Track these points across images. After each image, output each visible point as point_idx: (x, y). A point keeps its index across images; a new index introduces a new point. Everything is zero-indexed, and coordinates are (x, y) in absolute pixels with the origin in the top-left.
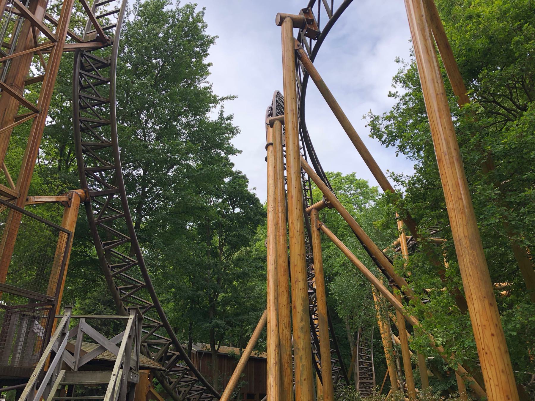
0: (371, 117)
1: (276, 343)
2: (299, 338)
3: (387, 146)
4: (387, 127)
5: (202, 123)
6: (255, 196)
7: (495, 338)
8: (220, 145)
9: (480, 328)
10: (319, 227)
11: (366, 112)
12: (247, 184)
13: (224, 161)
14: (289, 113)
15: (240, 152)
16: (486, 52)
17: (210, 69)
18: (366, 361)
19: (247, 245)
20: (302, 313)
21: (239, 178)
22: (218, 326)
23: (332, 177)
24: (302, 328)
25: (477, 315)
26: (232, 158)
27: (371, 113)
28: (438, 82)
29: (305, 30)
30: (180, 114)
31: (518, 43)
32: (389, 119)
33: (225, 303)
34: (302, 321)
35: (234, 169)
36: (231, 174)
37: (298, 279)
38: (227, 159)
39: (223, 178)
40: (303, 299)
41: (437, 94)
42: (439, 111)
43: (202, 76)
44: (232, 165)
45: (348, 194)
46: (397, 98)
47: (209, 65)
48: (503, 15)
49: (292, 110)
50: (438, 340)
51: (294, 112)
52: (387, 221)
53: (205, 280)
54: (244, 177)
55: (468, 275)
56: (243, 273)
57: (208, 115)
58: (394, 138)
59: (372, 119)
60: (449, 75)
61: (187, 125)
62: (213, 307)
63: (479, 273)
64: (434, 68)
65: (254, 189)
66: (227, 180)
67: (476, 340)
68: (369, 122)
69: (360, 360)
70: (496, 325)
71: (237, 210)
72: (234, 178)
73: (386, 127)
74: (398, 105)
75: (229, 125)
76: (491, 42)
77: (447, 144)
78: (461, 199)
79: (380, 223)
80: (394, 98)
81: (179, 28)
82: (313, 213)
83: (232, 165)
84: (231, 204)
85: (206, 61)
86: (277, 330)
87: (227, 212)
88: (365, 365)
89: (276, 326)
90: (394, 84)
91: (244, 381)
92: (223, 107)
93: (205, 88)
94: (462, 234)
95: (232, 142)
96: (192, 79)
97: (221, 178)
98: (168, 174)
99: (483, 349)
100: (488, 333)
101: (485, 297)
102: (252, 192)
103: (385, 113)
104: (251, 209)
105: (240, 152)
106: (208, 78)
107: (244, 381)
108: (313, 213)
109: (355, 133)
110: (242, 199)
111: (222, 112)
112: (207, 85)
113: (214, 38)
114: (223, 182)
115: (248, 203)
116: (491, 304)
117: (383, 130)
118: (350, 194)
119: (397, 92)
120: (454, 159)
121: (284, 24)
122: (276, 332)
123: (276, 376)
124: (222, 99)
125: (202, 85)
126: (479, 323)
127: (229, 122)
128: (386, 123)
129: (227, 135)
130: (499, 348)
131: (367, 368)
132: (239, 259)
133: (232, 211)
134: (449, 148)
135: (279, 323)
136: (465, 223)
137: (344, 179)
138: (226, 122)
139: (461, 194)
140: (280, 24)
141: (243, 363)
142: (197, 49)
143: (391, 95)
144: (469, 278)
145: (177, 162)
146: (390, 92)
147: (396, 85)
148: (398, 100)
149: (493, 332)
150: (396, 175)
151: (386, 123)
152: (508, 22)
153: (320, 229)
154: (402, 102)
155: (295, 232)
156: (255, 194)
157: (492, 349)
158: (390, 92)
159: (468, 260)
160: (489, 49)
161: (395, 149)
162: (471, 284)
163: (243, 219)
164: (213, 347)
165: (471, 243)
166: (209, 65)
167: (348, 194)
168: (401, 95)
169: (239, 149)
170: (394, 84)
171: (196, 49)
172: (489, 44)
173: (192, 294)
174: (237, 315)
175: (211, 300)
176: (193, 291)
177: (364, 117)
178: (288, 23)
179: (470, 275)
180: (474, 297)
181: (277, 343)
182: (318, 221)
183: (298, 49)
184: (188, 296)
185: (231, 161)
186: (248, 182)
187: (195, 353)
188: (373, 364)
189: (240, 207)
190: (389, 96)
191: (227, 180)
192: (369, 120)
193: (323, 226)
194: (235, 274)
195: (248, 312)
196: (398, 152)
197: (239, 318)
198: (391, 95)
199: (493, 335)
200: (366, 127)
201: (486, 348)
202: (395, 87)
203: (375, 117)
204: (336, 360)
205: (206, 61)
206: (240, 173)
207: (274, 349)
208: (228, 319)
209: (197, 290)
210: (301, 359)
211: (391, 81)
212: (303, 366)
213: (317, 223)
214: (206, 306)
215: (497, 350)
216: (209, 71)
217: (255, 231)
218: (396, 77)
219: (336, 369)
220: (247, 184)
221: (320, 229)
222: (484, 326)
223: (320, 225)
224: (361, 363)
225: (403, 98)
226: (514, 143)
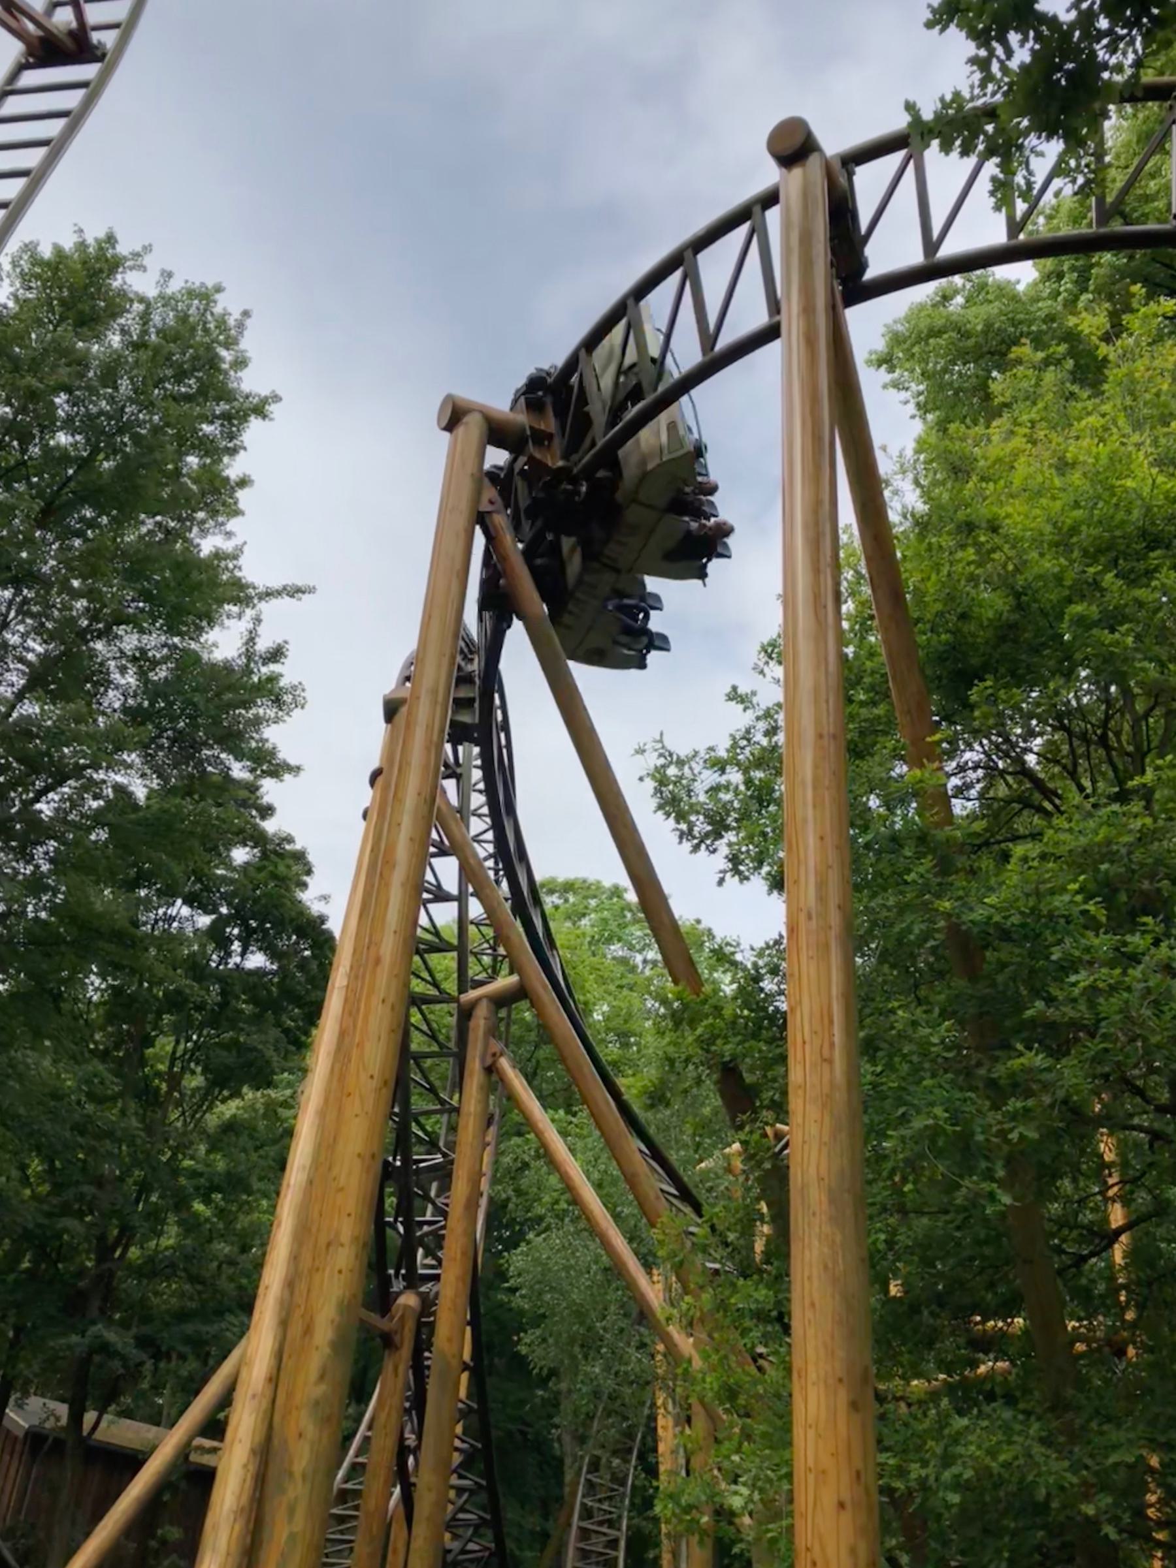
0: (661, 755)
1: (257, 1439)
2: (300, 1435)
3: (696, 848)
4: (714, 790)
5: (188, 662)
6: (323, 922)
7: (846, 1517)
8: (233, 741)
9: (811, 1478)
10: (489, 1061)
11: (647, 737)
12: (305, 878)
13: (244, 794)
14: (422, 699)
15: (296, 770)
16: (1006, 632)
17: (243, 497)
18: (604, 1529)
19: (263, 1080)
20: (327, 1350)
21: (281, 855)
22: (104, 1348)
23: (595, 897)
24: (317, 1403)
25: (811, 1433)
26: (270, 790)
27: (661, 741)
28: (827, 701)
29: (522, 459)
30: (121, 619)
31: (1081, 622)
32: (720, 766)
33: (152, 1269)
34: (322, 1378)
35: (270, 826)
36: (258, 839)
37: (337, 1234)
38: (253, 788)
39: (229, 846)
40: (340, 1304)
41: (821, 736)
42: (815, 788)
43: (214, 513)
44: (267, 811)
45: (639, 958)
46: (750, 712)
47: (243, 483)
48: (1064, 539)
49: (435, 692)
50: (736, 1493)
51: (440, 698)
52: (663, 1082)
53: (99, 1182)
54: (300, 857)
55: (807, 1302)
56: (228, 1174)
57: (212, 636)
58: (719, 827)
59: (662, 761)
60: (894, 678)
61: (141, 660)
62: (105, 1282)
63: (837, 1297)
64: (826, 659)
65: (325, 898)
66: (240, 855)
67: (796, 1515)
68: (652, 767)
69: (585, 1524)
70: (858, 1474)
71: (257, 960)
72: (265, 855)
73: (712, 789)
74: (748, 731)
75: (273, 679)
76: (1019, 607)
77: (821, 885)
78: (830, 1061)
79: (639, 1084)
80: (741, 707)
81: (154, 356)
82: (482, 1014)
83: (267, 811)
84: (239, 938)
85: (233, 469)
86: (269, 1393)
87: (223, 960)
88: (596, 1545)
89: (270, 1380)
90: (761, 664)
91: (174, 1557)
92: (258, 620)
93: (218, 555)
94: (812, 1171)
95: (273, 735)
96: (180, 519)
97: (216, 848)
98: (38, 806)
99: (808, 1549)
100: (828, 1500)
101: (840, 1380)
102: (316, 908)
103: (711, 749)
104: (303, 965)
105: (296, 770)
106: (233, 524)
107: (174, 1557)
108: (482, 1014)
109: (618, 794)
110: (281, 925)
111: (251, 639)
112: (228, 546)
113: (265, 401)
114: (228, 864)
115: (297, 943)
116: (854, 1406)
117: (702, 798)
118: (645, 961)
119: (754, 693)
120: (833, 934)
121: (460, 430)
122: (265, 1404)
123: (230, 1559)
124: (268, 594)
125: (207, 546)
126: (811, 1463)
127: (274, 667)
128: (710, 777)
129: (261, 711)
130: (853, 1551)
131: (602, 1554)
132: (230, 1127)
133: (238, 959)
134: (821, 899)
135: (282, 1374)
136: (826, 1139)
137: (630, 910)
138: (264, 670)
139: (832, 1045)
140: (450, 427)
141: (138, 1499)
142: (207, 428)
143: (734, 695)
144: (809, 1314)
145: (78, 772)
146: (735, 688)
147: (766, 670)
148: (750, 715)
149: (846, 1496)
150: (718, 940)
151: (710, 777)
152: (1072, 562)
153: (490, 1069)
154: (762, 726)
155: (364, 1077)
156: (322, 919)
157: (831, 1551)
158: (735, 688)
159: (815, 1252)
160: (1012, 626)
161: (719, 861)
162: (811, 1332)
163: (269, 992)
164: (76, 1418)
165: (832, 1201)
166: (243, 483)
167: (639, 958)
168: (763, 706)
169: (292, 762)
170: (761, 664)
171: (204, 426)
172: (1011, 611)
173: (39, 1226)
174: (183, 1316)
175: (104, 1251)
176: (49, 1215)
177: (641, 751)
178: (473, 427)
179: (813, 1305)
180: (812, 1376)
181: (259, 1437)
182: (493, 1041)
183: (489, 513)
184: (25, 1229)
185: (266, 800)
186: (309, 872)
187: (21, 1434)
188: (622, 1544)
189: (272, 953)
190: (730, 698)
191: (240, 855)
192: (653, 760)
193: (505, 1063)
194: (201, 1175)
195: (219, 1313)
196: (724, 872)
197: (189, 1328)
198: (734, 695)
199: (841, 1505)
200: (641, 779)
201: (817, 1548)
202: (762, 672)
203: (671, 755)
204: (480, 1518)
205: (233, 469)
206: (289, 839)
207: (244, 1460)
208: (146, 1330)
209: (65, 1210)
210: (291, 1511)
211: (753, 655)
212: (292, 1536)
213: (486, 1045)
214: (82, 1272)
215: (844, 1553)
216: (241, 505)
217: (303, 1038)
218: (770, 644)
219: (477, 1547)
220: (305, 878)
221: (490, 1069)
222: (824, 1472)
223: (494, 1055)
224: (585, 1534)
225: (767, 715)
226: (1018, 908)
